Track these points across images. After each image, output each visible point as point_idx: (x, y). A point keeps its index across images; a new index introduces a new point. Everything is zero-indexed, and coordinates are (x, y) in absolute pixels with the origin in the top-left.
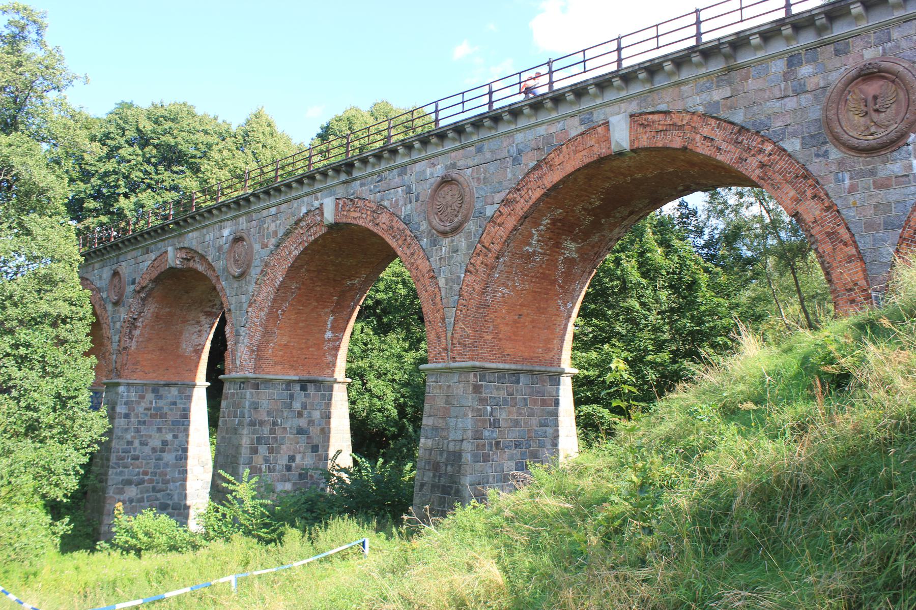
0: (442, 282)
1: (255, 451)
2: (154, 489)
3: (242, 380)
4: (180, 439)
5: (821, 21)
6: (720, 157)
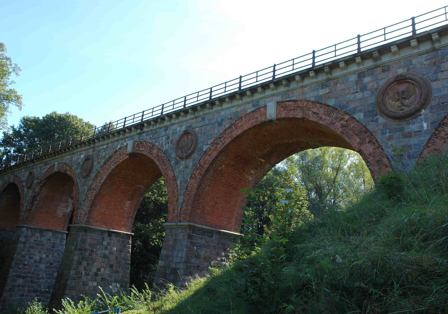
0: (179, 182)
1: (80, 263)
2: (32, 282)
3: (79, 227)
4: (49, 258)
5: (376, 54)
6: (321, 122)
